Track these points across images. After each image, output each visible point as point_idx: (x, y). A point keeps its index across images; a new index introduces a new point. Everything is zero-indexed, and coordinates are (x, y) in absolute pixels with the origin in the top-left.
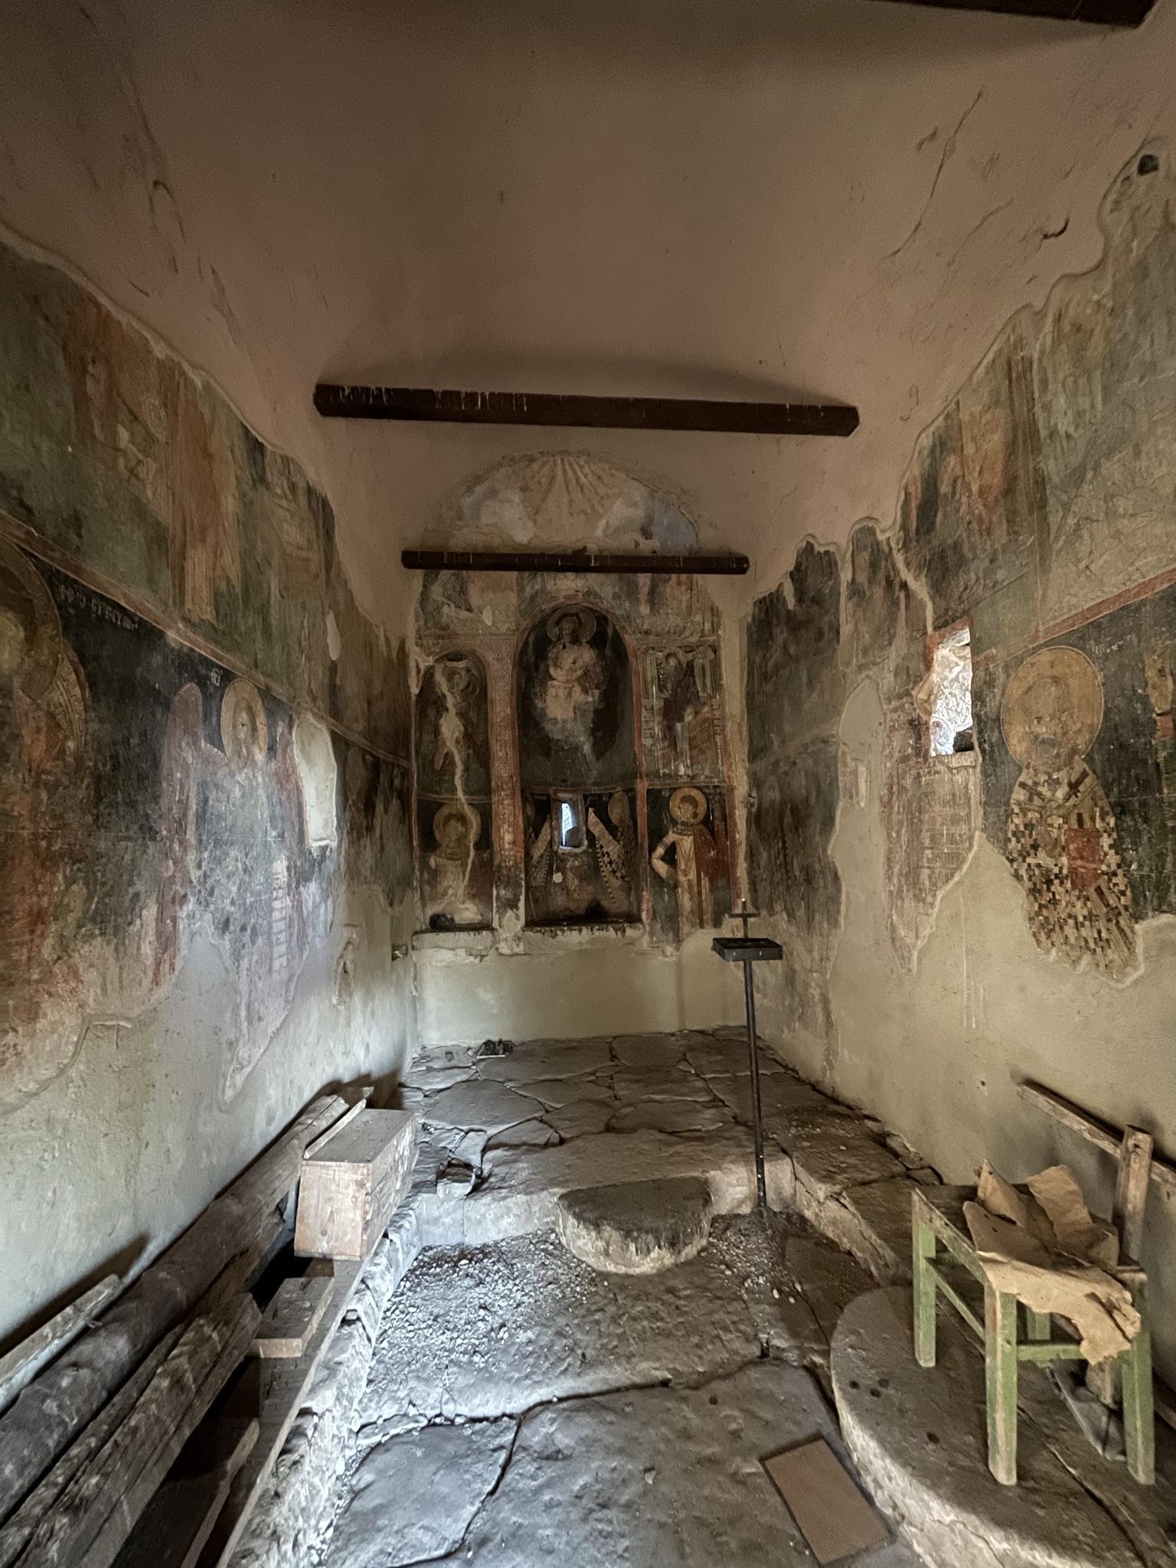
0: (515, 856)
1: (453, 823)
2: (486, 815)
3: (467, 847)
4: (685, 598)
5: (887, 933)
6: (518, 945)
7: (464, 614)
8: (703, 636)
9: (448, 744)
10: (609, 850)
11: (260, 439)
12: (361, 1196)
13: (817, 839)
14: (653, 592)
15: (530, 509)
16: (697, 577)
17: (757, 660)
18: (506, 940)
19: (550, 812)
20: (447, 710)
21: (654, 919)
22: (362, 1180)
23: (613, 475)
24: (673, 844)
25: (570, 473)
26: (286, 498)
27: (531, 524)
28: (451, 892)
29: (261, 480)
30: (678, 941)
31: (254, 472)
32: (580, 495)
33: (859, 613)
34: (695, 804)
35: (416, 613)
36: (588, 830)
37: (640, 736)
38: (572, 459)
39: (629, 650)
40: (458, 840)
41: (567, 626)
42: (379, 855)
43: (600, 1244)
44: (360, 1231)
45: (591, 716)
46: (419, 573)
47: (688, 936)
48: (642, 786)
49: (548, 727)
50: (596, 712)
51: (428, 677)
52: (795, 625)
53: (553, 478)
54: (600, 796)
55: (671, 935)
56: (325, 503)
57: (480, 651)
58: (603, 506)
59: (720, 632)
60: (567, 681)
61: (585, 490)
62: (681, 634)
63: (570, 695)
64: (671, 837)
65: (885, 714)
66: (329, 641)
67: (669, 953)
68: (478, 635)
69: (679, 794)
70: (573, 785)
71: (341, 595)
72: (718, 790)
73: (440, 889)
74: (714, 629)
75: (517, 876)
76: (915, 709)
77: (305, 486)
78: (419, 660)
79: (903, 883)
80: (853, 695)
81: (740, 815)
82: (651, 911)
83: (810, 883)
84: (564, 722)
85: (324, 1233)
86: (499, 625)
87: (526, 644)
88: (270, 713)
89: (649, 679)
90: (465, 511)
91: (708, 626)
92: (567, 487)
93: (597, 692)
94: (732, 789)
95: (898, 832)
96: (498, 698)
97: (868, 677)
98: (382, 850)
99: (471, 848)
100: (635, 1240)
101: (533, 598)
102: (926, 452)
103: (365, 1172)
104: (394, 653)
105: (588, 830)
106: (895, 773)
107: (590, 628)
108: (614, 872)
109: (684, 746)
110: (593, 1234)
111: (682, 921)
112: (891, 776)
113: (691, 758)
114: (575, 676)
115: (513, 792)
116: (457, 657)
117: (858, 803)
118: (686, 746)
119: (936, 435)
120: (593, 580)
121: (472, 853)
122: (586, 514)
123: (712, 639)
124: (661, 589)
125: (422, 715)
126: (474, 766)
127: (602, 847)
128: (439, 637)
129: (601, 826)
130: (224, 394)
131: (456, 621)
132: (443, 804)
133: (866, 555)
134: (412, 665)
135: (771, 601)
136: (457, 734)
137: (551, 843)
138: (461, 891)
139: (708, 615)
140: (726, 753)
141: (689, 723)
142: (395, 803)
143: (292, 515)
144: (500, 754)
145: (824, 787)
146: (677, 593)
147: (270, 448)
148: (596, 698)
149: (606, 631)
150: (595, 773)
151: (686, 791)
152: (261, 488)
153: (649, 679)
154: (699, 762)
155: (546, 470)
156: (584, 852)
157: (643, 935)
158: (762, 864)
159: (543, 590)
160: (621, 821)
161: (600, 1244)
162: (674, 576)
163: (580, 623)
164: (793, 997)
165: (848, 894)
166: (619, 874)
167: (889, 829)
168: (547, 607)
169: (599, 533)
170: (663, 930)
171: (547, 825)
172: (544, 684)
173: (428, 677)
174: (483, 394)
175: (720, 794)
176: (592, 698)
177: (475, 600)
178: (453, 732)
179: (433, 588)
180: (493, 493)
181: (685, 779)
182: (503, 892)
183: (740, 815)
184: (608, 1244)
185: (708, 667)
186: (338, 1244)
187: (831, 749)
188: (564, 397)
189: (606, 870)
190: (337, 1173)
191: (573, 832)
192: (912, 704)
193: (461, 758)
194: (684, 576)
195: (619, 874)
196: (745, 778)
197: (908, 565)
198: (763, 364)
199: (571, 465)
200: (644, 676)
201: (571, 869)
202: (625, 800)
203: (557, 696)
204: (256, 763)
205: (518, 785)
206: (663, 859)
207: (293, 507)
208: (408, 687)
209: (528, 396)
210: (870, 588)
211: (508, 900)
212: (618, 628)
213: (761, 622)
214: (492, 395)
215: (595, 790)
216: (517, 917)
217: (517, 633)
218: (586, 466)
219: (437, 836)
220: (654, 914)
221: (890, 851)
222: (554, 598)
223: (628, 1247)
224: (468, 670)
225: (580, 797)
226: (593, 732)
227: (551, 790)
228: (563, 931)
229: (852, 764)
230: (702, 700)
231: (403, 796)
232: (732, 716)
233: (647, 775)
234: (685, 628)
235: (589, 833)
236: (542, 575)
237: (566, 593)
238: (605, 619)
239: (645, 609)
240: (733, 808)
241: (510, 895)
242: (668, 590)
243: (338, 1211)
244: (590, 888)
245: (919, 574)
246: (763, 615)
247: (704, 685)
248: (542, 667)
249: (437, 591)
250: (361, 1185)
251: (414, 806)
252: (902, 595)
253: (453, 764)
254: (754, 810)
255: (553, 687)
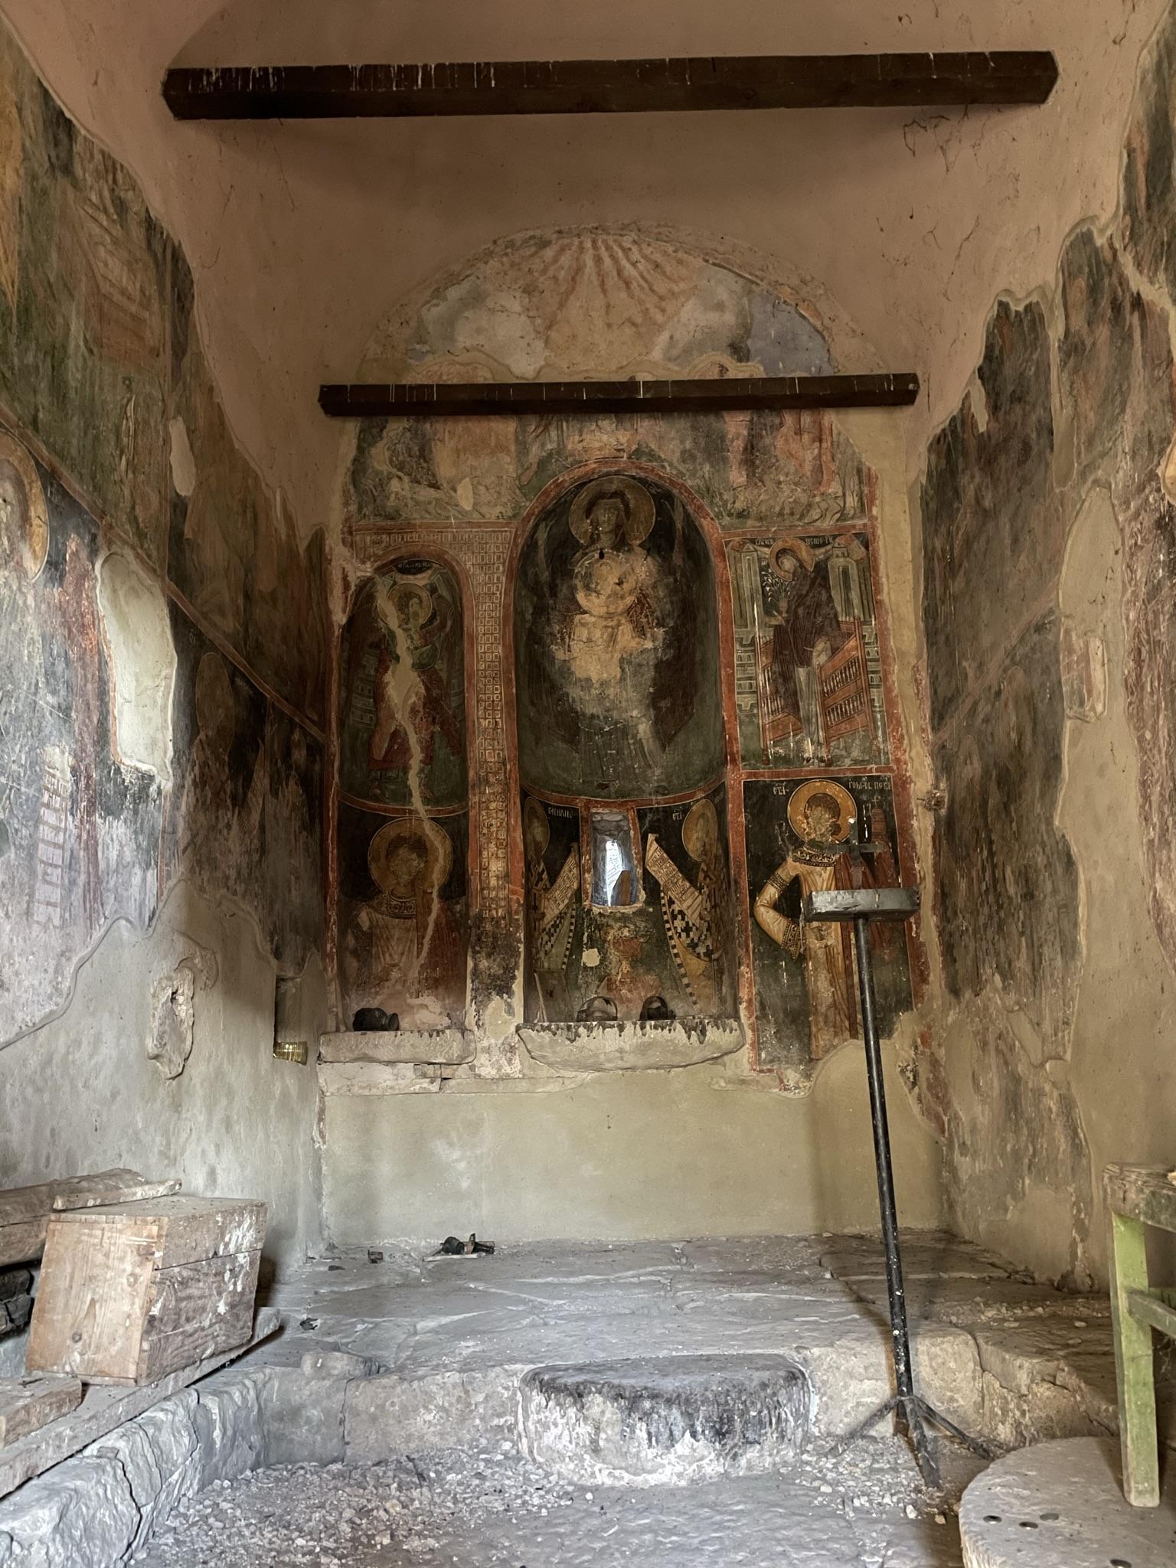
0: (509, 900)
1: (403, 852)
2: (459, 833)
3: (427, 894)
4: (809, 456)
5: (1149, 923)
6: (510, 1062)
7: (426, 493)
8: (843, 516)
9: (398, 716)
10: (684, 907)
11: (68, 115)
12: (146, 1273)
13: (1038, 809)
14: (751, 448)
15: (538, 321)
16: (831, 418)
17: (938, 545)
18: (488, 1050)
19: (576, 838)
20: (397, 658)
21: (763, 1016)
22: (149, 1246)
23: (680, 262)
24: (796, 881)
25: (605, 255)
26: (105, 211)
27: (539, 345)
28: (395, 974)
29: (65, 168)
30: (810, 1061)
31: (53, 154)
32: (623, 295)
33: (1079, 384)
34: (835, 809)
35: (345, 492)
36: (646, 872)
37: (731, 691)
38: (610, 241)
39: (712, 546)
40: (412, 883)
41: (605, 518)
42: (256, 857)
43: (584, 1430)
44: (137, 1335)
45: (650, 674)
46: (350, 429)
47: (827, 1051)
48: (735, 778)
49: (575, 692)
50: (659, 666)
51: (363, 599)
52: (989, 453)
53: (579, 270)
54: (667, 812)
55: (795, 1049)
56: (177, 256)
57: (451, 553)
58: (663, 311)
59: (875, 511)
60: (610, 616)
61: (634, 285)
62: (802, 516)
63: (613, 639)
64: (791, 868)
65: (1122, 530)
66: (174, 458)
67: (792, 1084)
68: (450, 526)
69: (805, 793)
70: (621, 793)
71: (198, 400)
72: (878, 785)
73: (377, 968)
74: (865, 505)
75: (509, 934)
76: (1163, 499)
77: (143, 214)
78: (349, 568)
79: (1167, 812)
80: (1075, 528)
81: (922, 827)
82: (756, 1004)
83: (1032, 896)
84: (603, 684)
85: (77, 1337)
86: (484, 510)
87: (531, 544)
88: (54, 510)
89: (747, 594)
90: (431, 328)
91: (851, 501)
92: (602, 284)
93: (660, 632)
94: (903, 783)
95: (1155, 732)
96: (481, 629)
97: (1096, 482)
98: (263, 850)
99: (435, 895)
100: (646, 1416)
101: (543, 463)
102: (1149, 78)
103: (155, 1229)
104: (302, 546)
105: (646, 872)
106: (1142, 625)
107: (646, 516)
108: (693, 946)
109: (811, 707)
110: (572, 1412)
111: (816, 1023)
112: (1137, 634)
113: (827, 728)
114: (622, 606)
115: (507, 789)
116: (412, 565)
117: (1093, 709)
118: (816, 708)
119: (1162, 44)
120: (646, 430)
121: (436, 906)
122: (634, 324)
123: (859, 522)
124: (767, 441)
125: (352, 663)
126: (442, 752)
127: (671, 902)
128: (380, 531)
129: (670, 863)
130: (10, 26)
131: (410, 503)
132: (385, 820)
133: (1082, 282)
134: (336, 577)
135: (954, 431)
136: (414, 699)
137: (578, 895)
138: (414, 973)
139: (853, 483)
140: (892, 719)
141: (821, 667)
142: (292, 791)
143: (115, 242)
144: (484, 723)
145: (1042, 708)
146: (794, 446)
147: (83, 132)
148: (659, 643)
149: (672, 523)
150: (658, 772)
151: (817, 786)
152: (63, 181)
153: (747, 594)
154: (841, 735)
155: (566, 260)
156: (640, 913)
157: (740, 1046)
158: (961, 904)
159: (560, 451)
160: (705, 852)
161: (584, 1430)
162: (789, 419)
163: (628, 512)
164: (1017, 1132)
165: (1089, 884)
166: (701, 950)
167: (1139, 727)
168: (566, 478)
169: (657, 354)
170: (780, 1040)
171: (571, 861)
172: (567, 619)
173: (363, 599)
174: (425, 67)
175: (882, 791)
176: (653, 643)
177: (444, 468)
178: (407, 697)
179: (373, 451)
180: (476, 299)
181: (815, 766)
182: (484, 964)
183: (922, 827)
184: (598, 1429)
185: (854, 572)
186: (99, 1357)
187: (1050, 637)
188: (556, 63)
189: (678, 944)
190: (107, 1234)
191: (625, 880)
192: (1158, 490)
193: (420, 741)
194: (807, 418)
195: (701, 950)
196: (928, 761)
197: (1138, 265)
198: (905, 20)
199: (608, 248)
200: (738, 588)
201: (617, 942)
202: (710, 813)
203: (589, 640)
204: (26, 574)
205: (515, 775)
206: (776, 907)
207: (117, 231)
208: (328, 613)
209: (497, 65)
210: (1091, 331)
211: (494, 978)
212: (690, 509)
213: (940, 475)
214: (440, 67)
215: (658, 801)
216: (510, 1010)
217: (515, 522)
218: (635, 249)
219: (375, 874)
220: (763, 1006)
221: (1145, 769)
222: (580, 463)
223: (633, 1432)
224: (433, 590)
225: (631, 814)
226: (654, 701)
227: (580, 803)
228: (590, 1029)
229: (1077, 643)
230: (843, 627)
231: (313, 789)
232: (902, 654)
233: (744, 759)
234: (810, 505)
235: (648, 879)
236: (560, 428)
237: (598, 454)
238: (669, 496)
239: (737, 476)
240: (907, 815)
241: (497, 970)
242: (780, 443)
243: (104, 1300)
244: (651, 979)
245: (1155, 274)
246: (943, 461)
247: (848, 601)
248: (564, 591)
249: (380, 457)
250: (145, 1254)
251: (332, 812)
252: (1135, 320)
253: (405, 750)
254: (943, 812)
255: (583, 625)
